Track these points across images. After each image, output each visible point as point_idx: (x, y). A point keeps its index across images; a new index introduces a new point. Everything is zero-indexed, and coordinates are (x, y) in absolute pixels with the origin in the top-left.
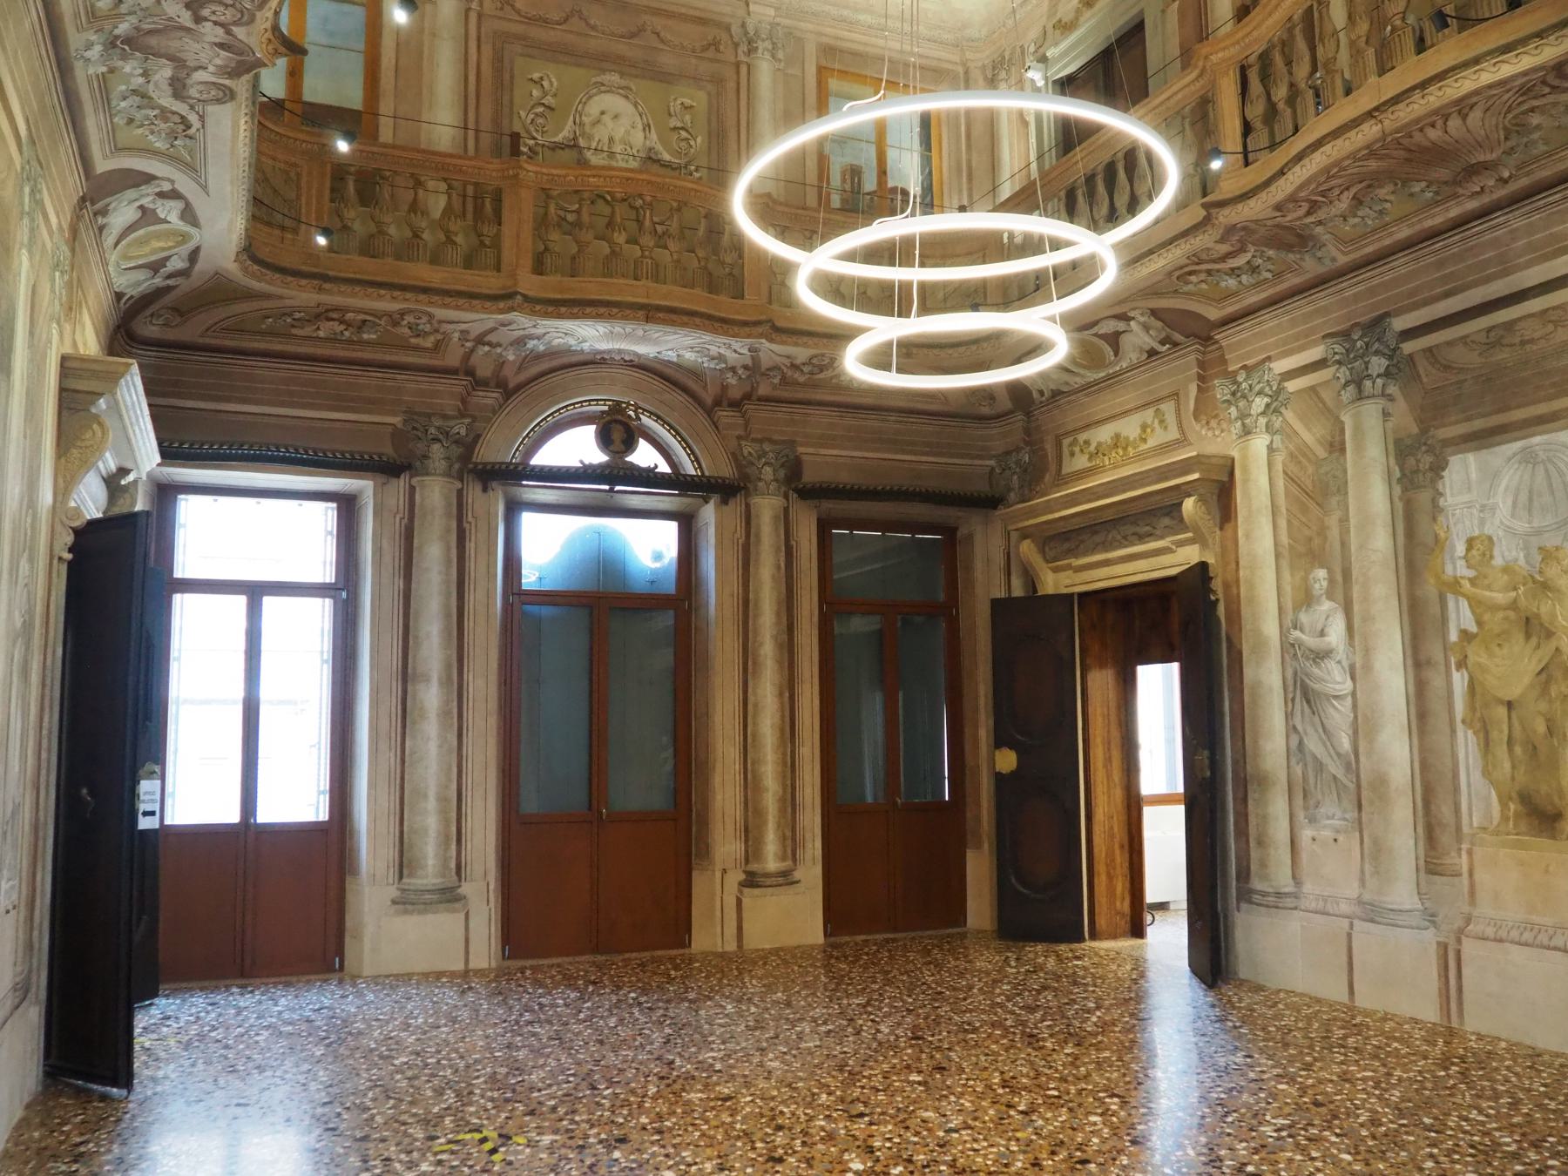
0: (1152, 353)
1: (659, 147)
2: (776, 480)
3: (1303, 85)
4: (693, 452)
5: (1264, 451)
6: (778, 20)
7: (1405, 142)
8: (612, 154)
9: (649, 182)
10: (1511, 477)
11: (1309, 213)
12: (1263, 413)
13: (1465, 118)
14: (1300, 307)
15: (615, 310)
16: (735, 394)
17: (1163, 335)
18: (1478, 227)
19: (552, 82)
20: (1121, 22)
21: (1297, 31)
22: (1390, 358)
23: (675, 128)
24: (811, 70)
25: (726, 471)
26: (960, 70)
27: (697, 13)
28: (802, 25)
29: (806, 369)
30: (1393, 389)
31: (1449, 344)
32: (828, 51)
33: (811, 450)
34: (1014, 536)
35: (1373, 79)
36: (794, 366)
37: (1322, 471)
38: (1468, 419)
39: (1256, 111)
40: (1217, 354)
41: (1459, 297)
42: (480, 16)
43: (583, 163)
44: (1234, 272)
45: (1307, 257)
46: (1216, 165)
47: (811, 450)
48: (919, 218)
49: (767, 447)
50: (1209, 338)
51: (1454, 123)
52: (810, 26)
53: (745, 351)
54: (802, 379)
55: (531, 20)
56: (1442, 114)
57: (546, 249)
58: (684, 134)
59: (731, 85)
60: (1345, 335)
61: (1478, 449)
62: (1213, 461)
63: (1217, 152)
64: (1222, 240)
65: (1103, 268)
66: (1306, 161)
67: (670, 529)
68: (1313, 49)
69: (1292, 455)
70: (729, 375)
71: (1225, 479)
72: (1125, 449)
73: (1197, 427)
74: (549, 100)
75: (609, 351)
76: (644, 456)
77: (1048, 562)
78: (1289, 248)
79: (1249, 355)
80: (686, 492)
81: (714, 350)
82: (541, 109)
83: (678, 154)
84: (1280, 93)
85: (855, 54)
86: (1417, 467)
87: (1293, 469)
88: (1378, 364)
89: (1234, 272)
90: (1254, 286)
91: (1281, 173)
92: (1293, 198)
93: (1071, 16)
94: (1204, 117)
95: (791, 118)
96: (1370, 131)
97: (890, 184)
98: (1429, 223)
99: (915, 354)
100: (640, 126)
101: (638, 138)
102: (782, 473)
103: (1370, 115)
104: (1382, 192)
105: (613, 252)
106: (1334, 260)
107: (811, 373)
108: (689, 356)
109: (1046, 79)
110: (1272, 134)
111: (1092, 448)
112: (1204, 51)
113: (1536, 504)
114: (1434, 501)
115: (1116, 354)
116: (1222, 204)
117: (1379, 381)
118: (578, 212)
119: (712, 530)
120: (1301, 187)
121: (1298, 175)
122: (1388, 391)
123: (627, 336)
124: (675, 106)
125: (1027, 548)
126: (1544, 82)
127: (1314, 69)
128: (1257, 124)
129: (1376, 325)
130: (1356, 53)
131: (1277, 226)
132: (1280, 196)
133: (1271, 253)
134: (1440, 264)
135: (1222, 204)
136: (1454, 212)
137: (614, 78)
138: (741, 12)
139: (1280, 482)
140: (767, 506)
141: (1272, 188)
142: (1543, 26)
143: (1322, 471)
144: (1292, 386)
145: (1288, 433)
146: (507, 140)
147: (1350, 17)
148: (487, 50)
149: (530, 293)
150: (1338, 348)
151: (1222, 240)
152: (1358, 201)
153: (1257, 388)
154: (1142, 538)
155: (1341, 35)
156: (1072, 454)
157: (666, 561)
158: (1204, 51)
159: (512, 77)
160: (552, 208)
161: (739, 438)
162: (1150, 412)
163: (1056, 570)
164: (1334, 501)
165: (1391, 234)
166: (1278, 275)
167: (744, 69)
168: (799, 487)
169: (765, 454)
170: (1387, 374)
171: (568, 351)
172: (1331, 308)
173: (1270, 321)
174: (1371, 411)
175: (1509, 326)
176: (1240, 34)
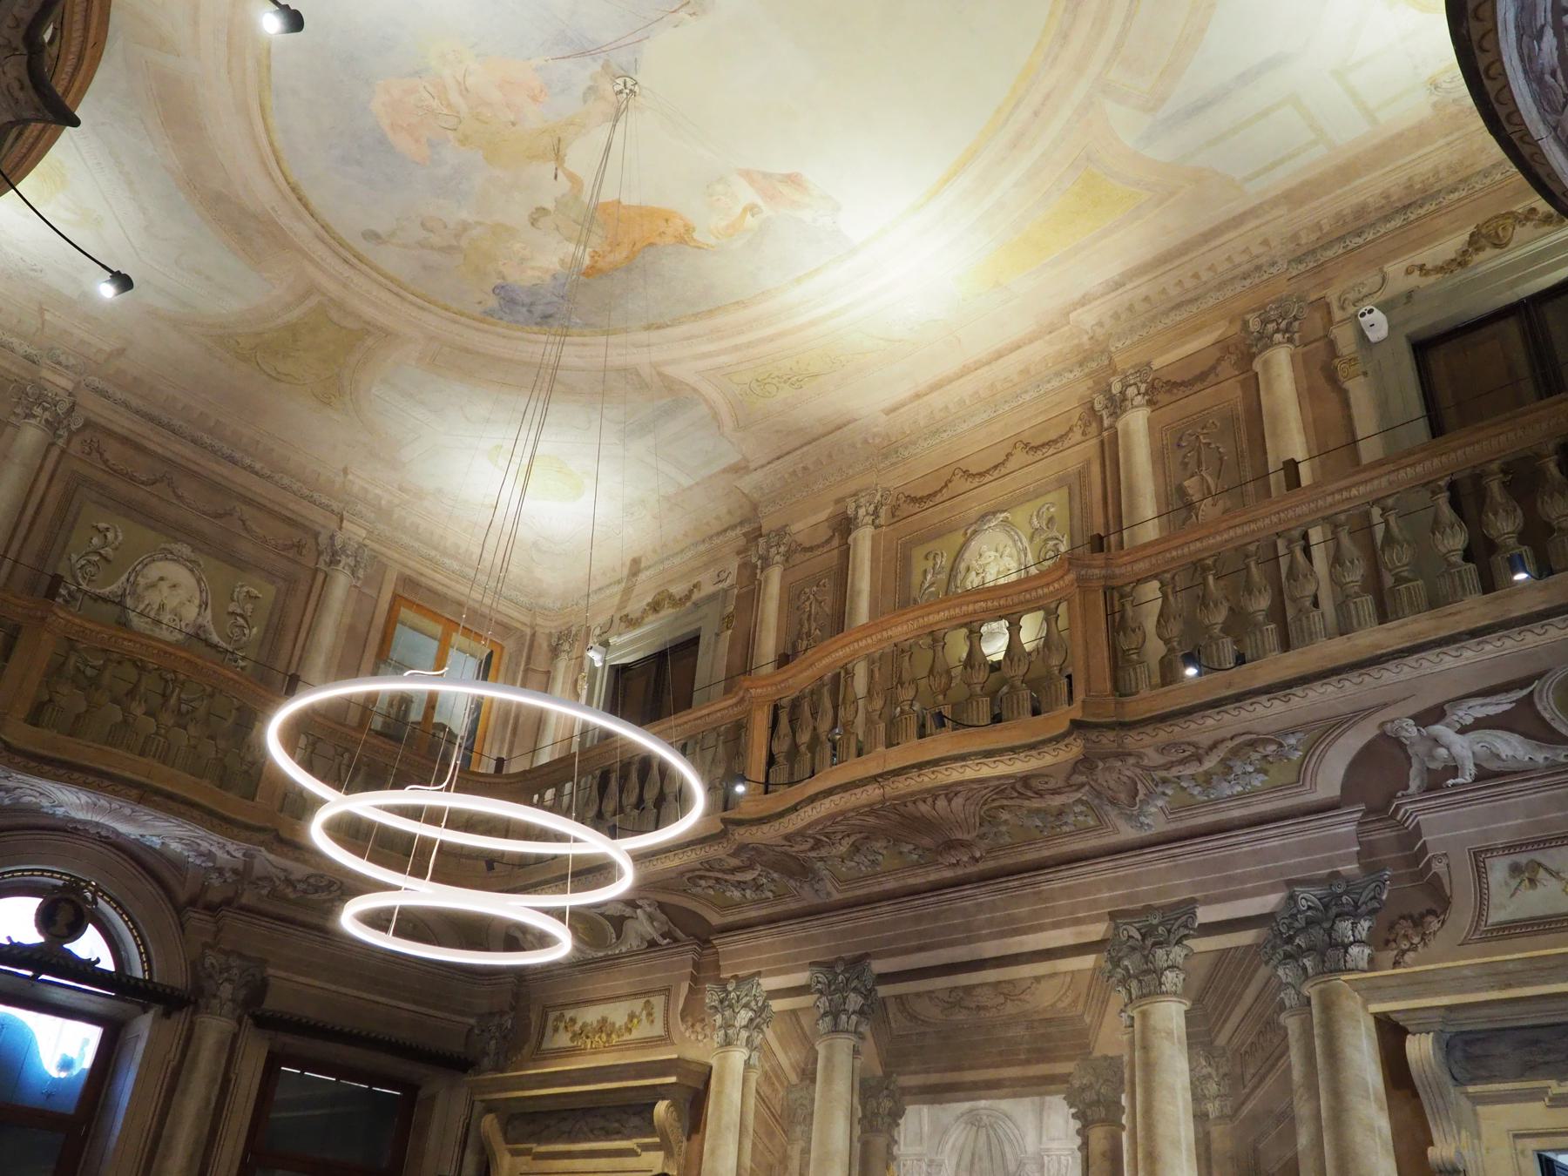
0: (652, 944)
1: (211, 628)
2: (233, 1000)
3: (823, 737)
4: (147, 952)
5: (740, 1067)
6: (367, 542)
7: (902, 808)
8: (158, 622)
9: (188, 661)
10: (957, 1135)
11: (812, 849)
12: (746, 1027)
13: (950, 801)
14: (796, 930)
15: (106, 783)
16: (214, 897)
17: (666, 929)
18: (951, 894)
19: (117, 535)
20: (678, 634)
21: (825, 690)
22: (866, 997)
23: (233, 613)
24: (386, 596)
25: (178, 979)
26: (528, 631)
27: (288, 514)
28: (390, 553)
29: (301, 886)
30: (865, 1029)
31: (918, 995)
32: (409, 583)
33: (283, 974)
34: (479, 1107)
35: (881, 749)
36: (289, 882)
37: (792, 1096)
38: (927, 1072)
39: (781, 747)
40: (712, 958)
41: (934, 953)
42: (63, 452)
43: (124, 624)
44: (740, 885)
45: (806, 887)
46: (740, 789)
47: (283, 974)
48: (451, 794)
49: (234, 962)
50: (710, 942)
51: (941, 803)
52: (396, 556)
53: (239, 855)
54: (292, 896)
55: (115, 472)
56: (933, 794)
57: (50, 700)
58: (241, 621)
59: (303, 588)
60: (829, 966)
61: (932, 1102)
62: (692, 1067)
63: (743, 779)
64: (733, 855)
65: (621, 875)
66: (817, 804)
67: (93, 1034)
68: (836, 708)
69: (766, 1074)
70: (214, 876)
71: (701, 1087)
72: (609, 1035)
73: (682, 1028)
74: (108, 551)
75: (85, 822)
76: (90, 946)
77: (507, 1142)
78: (791, 875)
79: (743, 966)
80: (118, 1001)
81: (205, 846)
82: (96, 558)
83: (229, 639)
84: (804, 738)
85: (430, 590)
86: (877, 1113)
87: (766, 1090)
88: (855, 1001)
89: (740, 885)
90: (754, 902)
91: (795, 809)
92: (801, 833)
93: (638, 614)
94: (737, 738)
95: (347, 669)
96: (872, 793)
97: (436, 719)
98: (911, 881)
99: (415, 924)
100: (197, 602)
101: (191, 613)
102: (242, 994)
103: (874, 779)
104: (878, 845)
105: (125, 721)
106: (829, 894)
107: (305, 892)
108: (175, 846)
109: (605, 662)
110: (792, 774)
111: (577, 1028)
112: (747, 684)
113: (977, 1167)
114: (889, 1147)
115: (618, 938)
116: (739, 823)
117: (854, 1018)
118: (101, 670)
119: (141, 1046)
120: (810, 826)
121: (809, 814)
122: (861, 1029)
123: (111, 811)
124: (240, 592)
125: (489, 1124)
126: (1013, 788)
127: (835, 726)
128: (781, 759)
129: (857, 963)
130: (869, 721)
131: (786, 853)
132: (791, 828)
133: (775, 875)
134: (918, 919)
135: (739, 823)
136: (933, 877)
137: (185, 550)
138: (334, 525)
139: (752, 1101)
140: (214, 1028)
141: (785, 820)
142: (1017, 743)
143: (792, 1096)
144: (777, 1005)
145: (765, 1050)
146: (46, 581)
147: (869, 691)
148: (57, 487)
149: (14, 743)
150: (822, 978)
151: (733, 855)
152: (856, 849)
153: (744, 1001)
154: (608, 1134)
155: (861, 703)
156: (556, 1030)
157: (75, 1072)
158: (747, 684)
159: (75, 520)
160: (72, 661)
161: (205, 945)
162: (640, 1003)
163: (515, 1153)
164: (799, 1129)
165: (880, 883)
166: (777, 896)
167: (320, 577)
168: (256, 1011)
169: (228, 969)
170: (861, 1012)
171: (35, 811)
172: (823, 937)
173: (765, 938)
174: (844, 1044)
175: (968, 989)
176: (779, 678)
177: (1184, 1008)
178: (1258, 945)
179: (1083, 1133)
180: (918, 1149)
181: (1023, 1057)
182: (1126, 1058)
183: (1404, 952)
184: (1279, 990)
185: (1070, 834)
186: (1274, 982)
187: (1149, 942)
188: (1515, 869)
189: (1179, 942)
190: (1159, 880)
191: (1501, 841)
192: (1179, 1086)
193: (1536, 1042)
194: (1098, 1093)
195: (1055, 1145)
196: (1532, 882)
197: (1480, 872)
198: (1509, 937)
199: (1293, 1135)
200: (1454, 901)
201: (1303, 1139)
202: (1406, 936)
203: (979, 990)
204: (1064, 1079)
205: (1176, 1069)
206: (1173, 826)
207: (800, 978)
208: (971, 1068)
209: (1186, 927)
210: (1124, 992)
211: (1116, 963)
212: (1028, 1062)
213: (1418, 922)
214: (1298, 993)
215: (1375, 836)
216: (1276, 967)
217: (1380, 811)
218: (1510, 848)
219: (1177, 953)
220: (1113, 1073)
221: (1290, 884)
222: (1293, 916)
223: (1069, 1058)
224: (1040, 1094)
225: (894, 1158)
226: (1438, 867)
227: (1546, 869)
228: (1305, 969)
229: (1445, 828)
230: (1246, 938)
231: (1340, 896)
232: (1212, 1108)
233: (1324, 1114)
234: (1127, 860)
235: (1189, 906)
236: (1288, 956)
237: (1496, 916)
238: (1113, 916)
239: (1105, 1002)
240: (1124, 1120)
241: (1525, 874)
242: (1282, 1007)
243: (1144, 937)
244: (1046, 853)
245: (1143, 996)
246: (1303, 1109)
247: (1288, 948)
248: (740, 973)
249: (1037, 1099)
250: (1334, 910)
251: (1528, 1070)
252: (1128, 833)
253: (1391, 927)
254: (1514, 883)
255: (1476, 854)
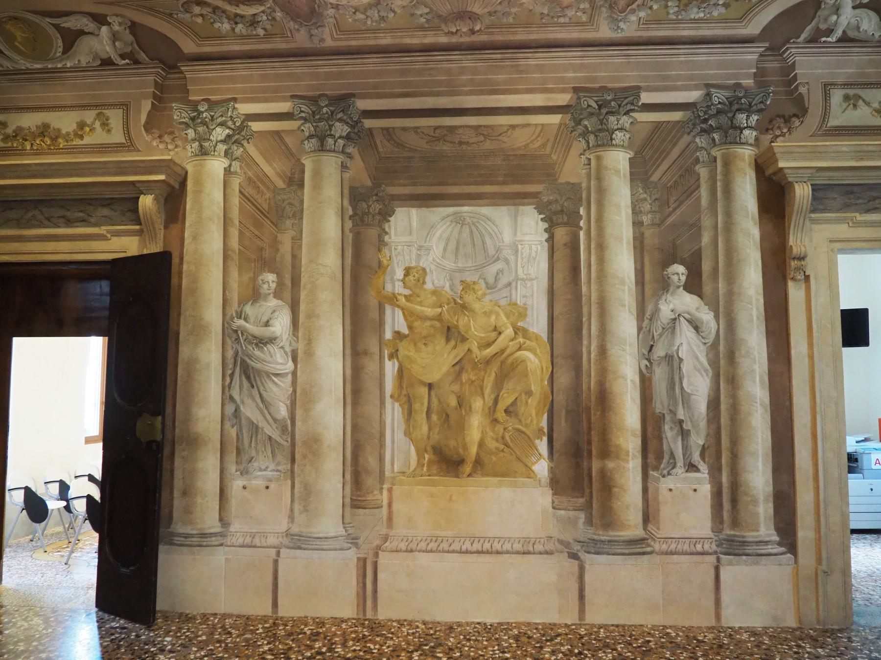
0: (107, 63)
12: (223, 141)
14: (278, 68)
31: (404, 129)
38: (415, 184)
50: (178, 68)
60: (313, 100)
73: (148, 138)
87: (250, 191)
88: (340, 129)
89: (236, 19)
90: (242, 37)
98: (407, 41)
106: (322, 40)
115: (64, 53)
117: (341, 142)
129: (342, 101)
134: (403, 73)
139: (235, 200)
144: (256, 126)
153: (220, 120)
164: (289, 223)
165: (376, 38)
170: (348, 138)
172: (306, 76)
174: (331, 164)
175: (452, 129)
177: (629, 156)
178: (683, 122)
179: (550, 232)
180: (407, 239)
181: (500, 179)
182: (584, 185)
183: (777, 137)
184: (696, 151)
185: (563, 25)
186: (693, 146)
187: (604, 111)
188: (847, 98)
189: (627, 113)
190: (613, 70)
191: (840, 80)
192: (623, 204)
193: (852, 193)
194: (562, 206)
195: (527, 238)
196: (855, 106)
197: (827, 97)
198: (838, 135)
199: (698, 236)
200: (809, 111)
201: (706, 239)
202: (779, 128)
203: (461, 131)
204: (535, 195)
205: (621, 195)
206: (639, 34)
207: (284, 107)
208: (454, 184)
209: (632, 104)
210: (584, 142)
211: (578, 122)
212: (504, 183)
213: (787, 120)
214: (709, 154)
215: (768, 65)
216: (695, 137)
217: (775, 50)
218: (845, 85)
219: (625, 121)
220: (574, 193)
221: (708, 86)
222: (708, 107)
223: (540, 182)
224: (514, 205)
225: (386, 244)
226: (803, 90)
227: (864, 100)
228: (714, 140)
229: (810, 66)
230: (676, 116)
231: (740, 98)
232: (646, 219)
233: (720, 226)
234: (593, 52)
235: (636, 91)
236: (703, 131)
237: (833, 122)
238: (576, 90)
239: (569, 148)
240: (582, 223)
241: (851, 101)
242: (697, 161)
243: (600, 107)
244: (534, 37)
245: (598, 146)
246: (706, 222)
247: (704, 126)
248: (213, 98)
249: (512, 208)
250: (736, 107)
251: (846, 207)
252: (605, 32)
253: (771, 121)
254: (845, 105)
255: (826, 85)
